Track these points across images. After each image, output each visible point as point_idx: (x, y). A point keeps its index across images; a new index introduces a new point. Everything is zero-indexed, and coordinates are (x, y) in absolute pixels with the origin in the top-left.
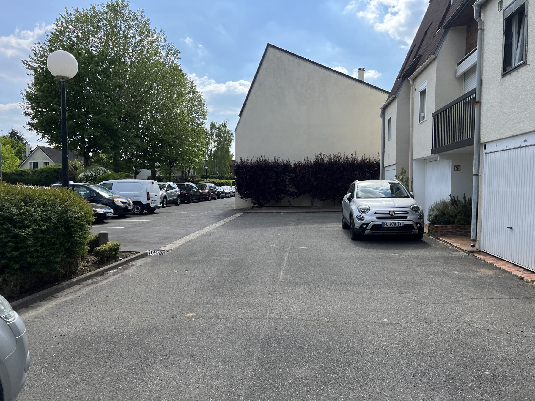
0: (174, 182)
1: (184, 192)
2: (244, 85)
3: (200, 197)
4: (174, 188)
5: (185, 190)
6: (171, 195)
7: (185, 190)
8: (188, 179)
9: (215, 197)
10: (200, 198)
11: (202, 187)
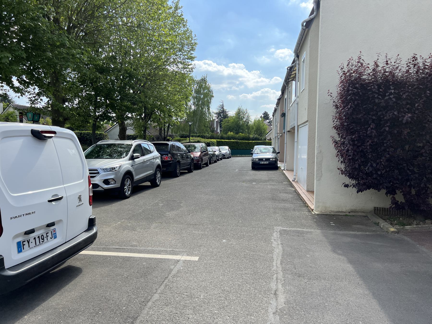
0: (151, 139)
1: (168, 158)
2: (207, 64)
3: (190, 164)
4: (150, 152)
5: (169, 155)
6: (144, 166)
7: (169, 155)
8: (166, 137)
9: (208, 162)
10: (191, 167)
11: (190, 149)
